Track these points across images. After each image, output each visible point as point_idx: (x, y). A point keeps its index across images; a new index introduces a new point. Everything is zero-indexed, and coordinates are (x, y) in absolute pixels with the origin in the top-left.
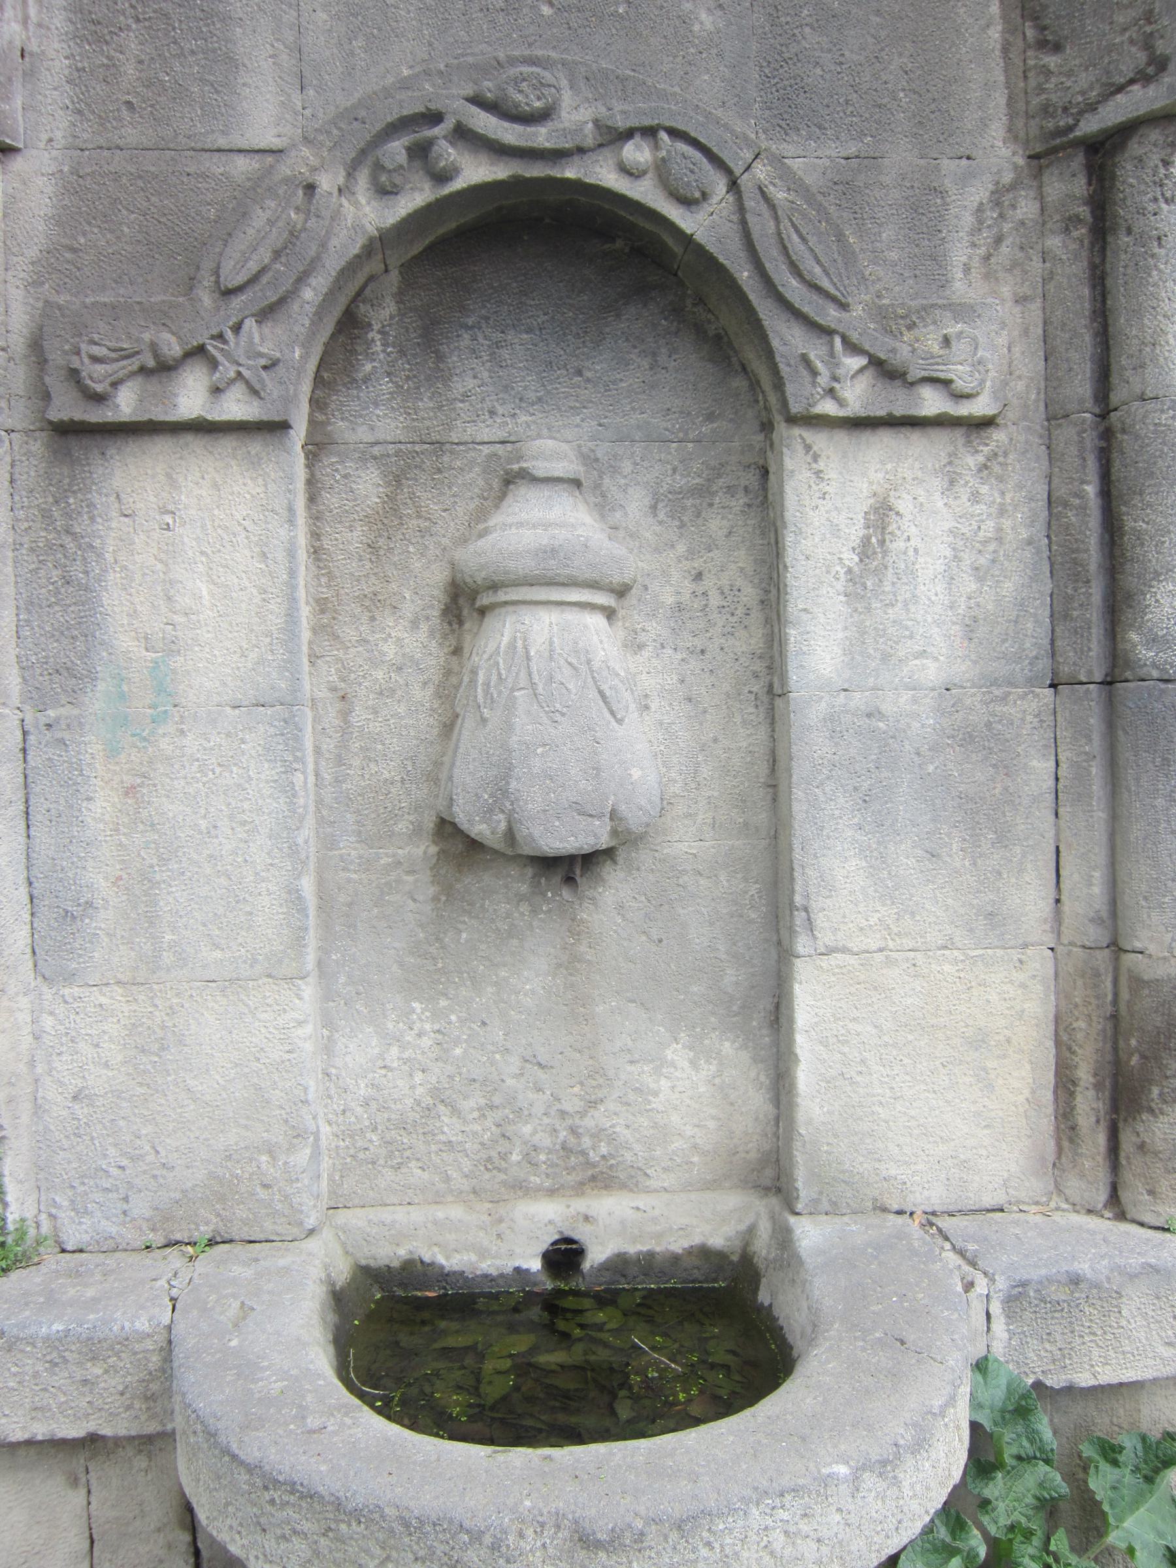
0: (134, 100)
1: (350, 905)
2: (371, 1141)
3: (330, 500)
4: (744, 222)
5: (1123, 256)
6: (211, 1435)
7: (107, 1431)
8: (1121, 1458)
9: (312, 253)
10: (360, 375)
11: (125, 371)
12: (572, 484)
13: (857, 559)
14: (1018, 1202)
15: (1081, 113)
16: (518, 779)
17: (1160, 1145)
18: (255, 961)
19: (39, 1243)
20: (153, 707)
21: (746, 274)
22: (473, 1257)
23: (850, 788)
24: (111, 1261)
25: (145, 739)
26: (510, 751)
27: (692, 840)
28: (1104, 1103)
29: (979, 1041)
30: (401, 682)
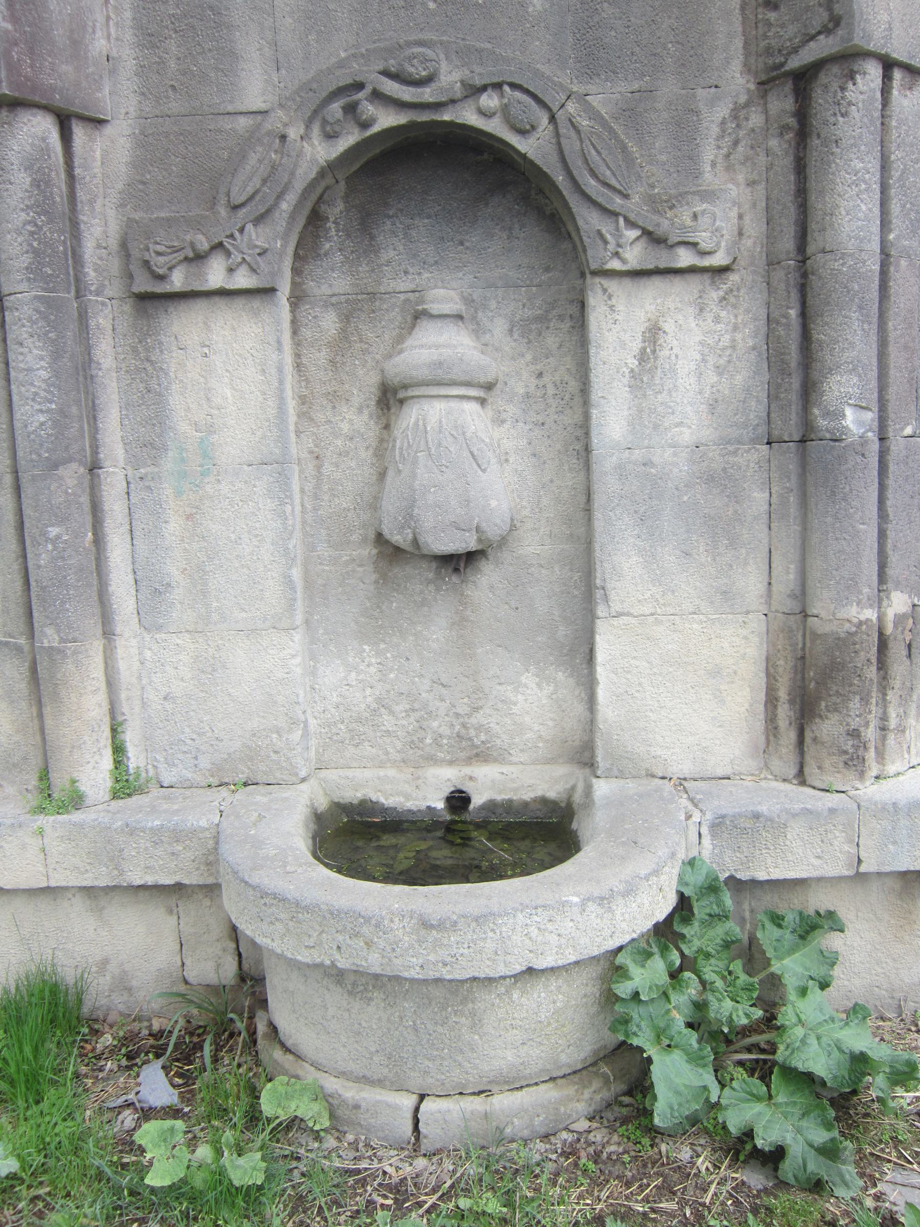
0: (176, 85)
1: (324, 585)
2: (340, 729)
3: (306, 333)
4: (559, 143)
5: (815, 154)
6: (236, 873)
7: (186, 881)
8: (784, 924)
9: (286, 180)
10: (322, 251)
11: (176, 260)
12: (456, 320)
13: (637, 363)
14: (740, 774)
15: (789, 54)
16: (419, 508)
17: (825, 738)
18: (266, 619)
19: (148, 782)
20: (201, 466)
21: (561, 178)
22: (402, 799)
23: (632, 511)
24: (188, 792)
25: (197, 486)
26: (415, 491)
27: (535, 545)
28: (795, 713)
29: (716, 672)
30: (353, 447)
